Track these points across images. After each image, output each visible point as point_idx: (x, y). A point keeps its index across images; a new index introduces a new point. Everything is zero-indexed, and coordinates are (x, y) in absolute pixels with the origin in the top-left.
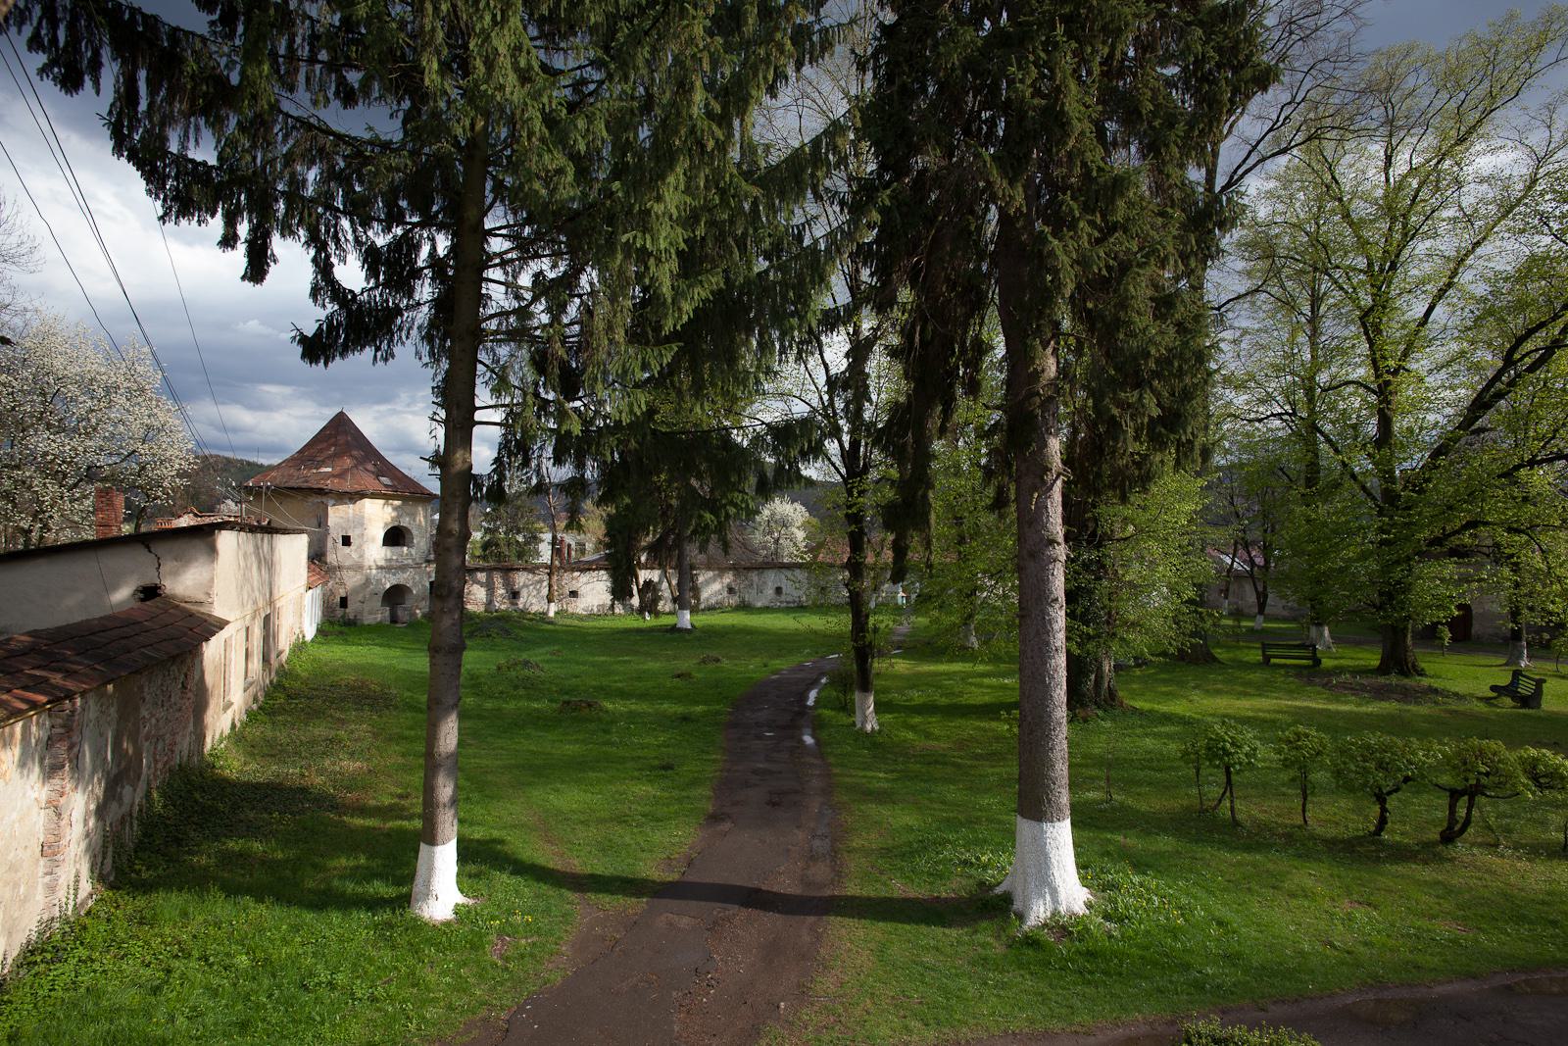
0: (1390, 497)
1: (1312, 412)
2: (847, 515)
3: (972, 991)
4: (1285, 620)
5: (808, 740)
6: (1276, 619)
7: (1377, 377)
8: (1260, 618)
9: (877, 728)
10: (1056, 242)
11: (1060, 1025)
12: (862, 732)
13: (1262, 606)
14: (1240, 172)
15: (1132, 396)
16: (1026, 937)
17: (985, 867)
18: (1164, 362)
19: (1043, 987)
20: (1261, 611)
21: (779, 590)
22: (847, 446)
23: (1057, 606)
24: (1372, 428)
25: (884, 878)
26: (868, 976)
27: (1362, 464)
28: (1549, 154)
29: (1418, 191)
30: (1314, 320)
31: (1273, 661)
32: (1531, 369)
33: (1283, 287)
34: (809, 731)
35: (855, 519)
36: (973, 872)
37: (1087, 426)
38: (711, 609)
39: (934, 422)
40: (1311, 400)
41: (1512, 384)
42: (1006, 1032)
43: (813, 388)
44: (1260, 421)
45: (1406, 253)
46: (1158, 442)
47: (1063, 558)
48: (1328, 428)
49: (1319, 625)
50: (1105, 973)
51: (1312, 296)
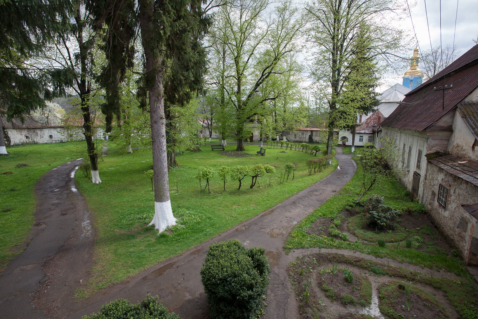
0: (240, 107)
1: (223, 82)
2: (82, 108)
3: (147, 255)
4: (216, 139)
5: (74, 190)
6: (214, 139)
7: (238, 75)
8: (210, 139)
9: (101, 182)
10: (165, 17)
11: (173, 256)
12: (95, 184)
13: (211, 135)
14: (207, 9)
15: (186, 74)
16: (161, 235)
17: (145, 219)
18: (195, 64)
19: (167, 247)
20: (210, 137)
21: (51, 137)
22: (80, 82)
23: (164, 138)
24: (236, 89)
25: (112, 229)
26: (112, 261)
27: (234, 98)
28: (270, 25)
29: (247, 27)
30: (224, 58)
31: (214, 150)
32: (266, 77)
33: (217, 46)
34: (74, 186)
35: (86, 109)
36: (141, 221)
37: (171, 82)
38: (16, 145)
39: (119, 75)
40: (223, 80)
41: (263, 81)
42: (159, 262)
43: (62, 57)
44: (211, 84)
45: (244, 43)
46: (192, 89)
47: (165, 123)
48: (226, 88)
49: (224, 140)
50: (183, 239)
51: (224, 50)
